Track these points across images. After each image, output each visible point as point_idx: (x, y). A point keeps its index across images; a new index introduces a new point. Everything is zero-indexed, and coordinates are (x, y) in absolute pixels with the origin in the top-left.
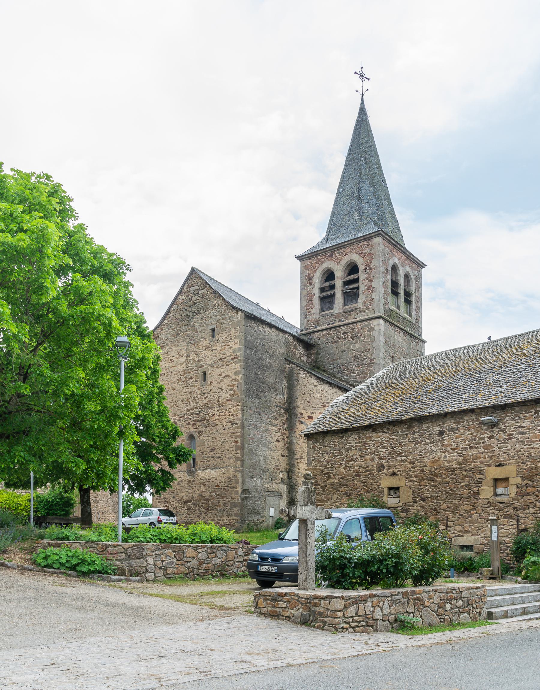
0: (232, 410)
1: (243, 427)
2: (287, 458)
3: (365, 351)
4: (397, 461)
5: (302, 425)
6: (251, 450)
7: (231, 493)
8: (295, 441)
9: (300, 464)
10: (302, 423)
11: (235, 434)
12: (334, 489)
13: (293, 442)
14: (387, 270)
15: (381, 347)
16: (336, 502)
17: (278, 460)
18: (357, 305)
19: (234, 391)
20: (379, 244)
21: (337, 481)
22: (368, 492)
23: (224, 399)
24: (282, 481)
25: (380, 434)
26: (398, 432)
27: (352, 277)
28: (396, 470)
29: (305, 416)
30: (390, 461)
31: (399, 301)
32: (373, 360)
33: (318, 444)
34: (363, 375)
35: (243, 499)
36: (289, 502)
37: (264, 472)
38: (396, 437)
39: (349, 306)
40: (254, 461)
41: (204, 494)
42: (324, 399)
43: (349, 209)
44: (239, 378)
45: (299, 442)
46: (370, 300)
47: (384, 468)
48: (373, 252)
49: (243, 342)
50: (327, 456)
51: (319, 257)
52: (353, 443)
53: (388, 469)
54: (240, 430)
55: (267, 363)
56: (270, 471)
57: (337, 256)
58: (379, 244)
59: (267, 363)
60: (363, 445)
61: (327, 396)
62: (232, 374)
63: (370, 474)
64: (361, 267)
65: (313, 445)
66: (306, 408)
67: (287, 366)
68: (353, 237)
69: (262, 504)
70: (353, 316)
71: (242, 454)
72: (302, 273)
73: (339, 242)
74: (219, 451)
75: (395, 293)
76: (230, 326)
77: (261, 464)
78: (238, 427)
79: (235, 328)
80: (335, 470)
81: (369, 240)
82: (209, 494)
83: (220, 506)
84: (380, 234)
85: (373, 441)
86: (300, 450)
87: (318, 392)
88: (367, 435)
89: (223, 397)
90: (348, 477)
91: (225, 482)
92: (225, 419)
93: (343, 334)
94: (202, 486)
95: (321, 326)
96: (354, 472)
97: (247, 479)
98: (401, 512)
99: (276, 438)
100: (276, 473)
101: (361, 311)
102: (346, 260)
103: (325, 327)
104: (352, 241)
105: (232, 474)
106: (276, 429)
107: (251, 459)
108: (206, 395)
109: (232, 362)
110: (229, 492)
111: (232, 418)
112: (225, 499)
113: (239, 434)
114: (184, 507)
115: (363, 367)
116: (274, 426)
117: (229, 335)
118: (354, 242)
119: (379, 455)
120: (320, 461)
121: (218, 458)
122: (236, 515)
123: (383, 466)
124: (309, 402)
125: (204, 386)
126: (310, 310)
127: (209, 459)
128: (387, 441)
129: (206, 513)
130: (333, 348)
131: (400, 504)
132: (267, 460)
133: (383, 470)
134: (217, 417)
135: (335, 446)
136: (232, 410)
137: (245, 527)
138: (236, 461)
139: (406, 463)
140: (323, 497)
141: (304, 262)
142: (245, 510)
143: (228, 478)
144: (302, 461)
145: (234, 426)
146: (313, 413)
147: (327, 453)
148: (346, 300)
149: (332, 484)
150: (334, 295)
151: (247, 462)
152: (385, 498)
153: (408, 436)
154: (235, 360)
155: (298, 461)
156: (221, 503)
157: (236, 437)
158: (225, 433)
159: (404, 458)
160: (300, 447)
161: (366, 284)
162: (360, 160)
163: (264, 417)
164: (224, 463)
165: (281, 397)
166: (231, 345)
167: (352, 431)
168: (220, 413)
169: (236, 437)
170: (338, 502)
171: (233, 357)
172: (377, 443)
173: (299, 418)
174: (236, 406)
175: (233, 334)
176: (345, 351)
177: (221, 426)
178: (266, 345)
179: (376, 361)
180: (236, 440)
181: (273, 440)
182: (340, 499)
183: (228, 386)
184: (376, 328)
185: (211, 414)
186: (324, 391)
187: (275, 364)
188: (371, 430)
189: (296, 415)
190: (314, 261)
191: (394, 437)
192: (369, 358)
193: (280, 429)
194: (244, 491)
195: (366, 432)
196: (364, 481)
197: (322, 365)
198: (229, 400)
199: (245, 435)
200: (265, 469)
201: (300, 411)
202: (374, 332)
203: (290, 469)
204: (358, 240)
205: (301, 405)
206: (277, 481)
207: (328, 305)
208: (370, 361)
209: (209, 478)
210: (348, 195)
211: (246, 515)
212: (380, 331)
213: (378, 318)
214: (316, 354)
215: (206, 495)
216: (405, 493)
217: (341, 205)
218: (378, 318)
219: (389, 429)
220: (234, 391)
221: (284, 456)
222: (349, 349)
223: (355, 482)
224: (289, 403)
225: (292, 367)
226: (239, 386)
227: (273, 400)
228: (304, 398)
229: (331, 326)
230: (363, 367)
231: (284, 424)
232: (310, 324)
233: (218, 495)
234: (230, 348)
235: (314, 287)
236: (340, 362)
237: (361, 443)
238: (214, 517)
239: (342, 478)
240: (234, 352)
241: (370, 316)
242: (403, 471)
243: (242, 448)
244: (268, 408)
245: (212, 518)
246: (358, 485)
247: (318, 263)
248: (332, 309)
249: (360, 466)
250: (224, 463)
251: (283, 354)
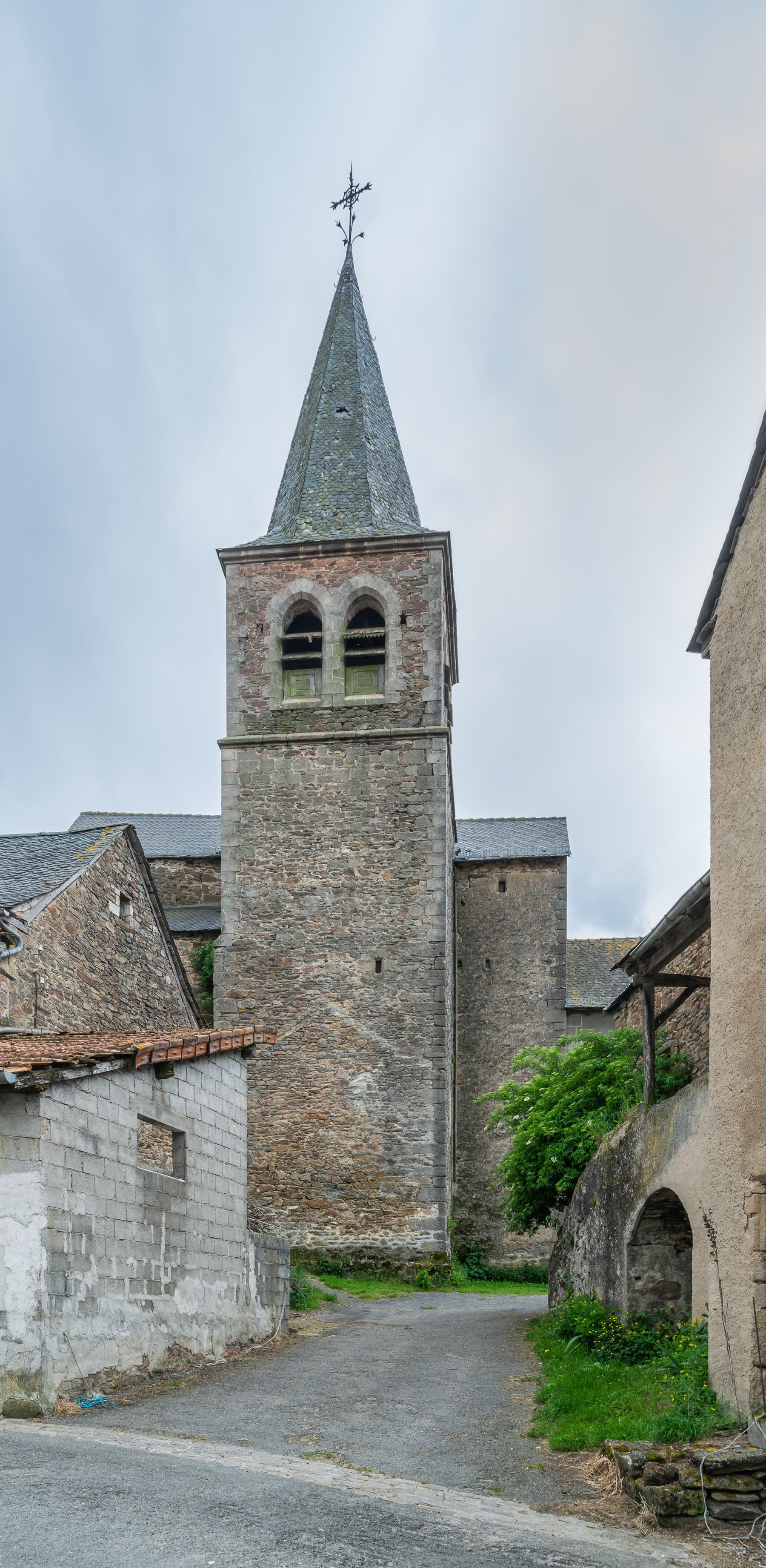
64: (392, 619)
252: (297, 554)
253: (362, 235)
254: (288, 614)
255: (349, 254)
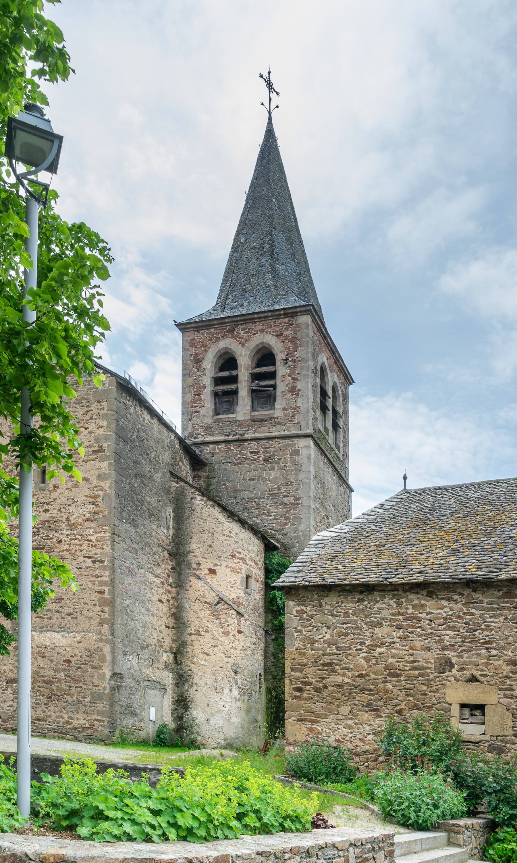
0: (93, 538)
1: (113, 569)
2: (174, 631)
3: (285, 484)
4: (479, 655)
5: (199, 581)
6: (125, 609)
7: (92, 677)
8: (188, 606)
9: (196, 643)
10: (199, 578)
11: (98, 579)
12: (343, 694)
13: (183, 607)
14: (316, 368)
15: (311, 481)
16: (347, 719)
17: (161, 632)
18: (272, 412)
19: (97, 506)
20: (308, 325)
21: (350, 681)
22: (416, 707)
23: (78, 517)
24: (166, 667)
25: (444, 603)
26: (482, 602)
27: (264, 369)
28: (477, 674)
29: (205, 567)
30: (465, 656)
31: (327, 422)
32: (299, 499)
33: (309, 608)
34: (283, 520)
35: (113, 689)
36: (177, 701)
37: (142, 648)
38: (478, 612)
39: (260, 413)
40: (129, 627)
41: (42, 672)
42: (234, 546)
43: (257, 268)
44: (106, 485)
45: (194, 608)
46: (293, 408)
47: (452, 666)
48: (298, 336)
49: (114, 426)
50: (329, 631)
51: (212, 330)
52: (385, 613)
53: (462, 669)
54: (107, 573)
55: (147, 472)
56: (150, 648)
57: (242, 333)
58: (308, 325)
59: (147, 472)
60: (407, 619)
61: (237, 542)
62: (93, 478)
63: (420, 675)
64: (280, 357)
65: (297, 608)
66: (206, 556)
67: (174, 484)
68: (267, 309)
69: (140, 699)
70: (266, 429)
71: (112, 614)
72: (184, 350)
73: (244, 312)
74: (70, 604)
75: (324, 408)
76: (91, 396)
77: (138, 635)
78: (104, 568)
79: (99, 401)
80: (346, 660)
81: (293, 317)
82: (52, 673)
83: (72, 695)
84: (310, 310)
85: (428, 614)
86: (196, 621)
87: (225, 532)
88: (416, 602)
89: (77, 515)
90: (373, 676)
91: (81, 656)
92: (81, 551)
93: (251, 453)
94: (39, 659)
95: (215, 435)
96: (387, 667)
97: (120, 657)
98: (488, 752)
99: (158, 597)
100: (159, 652)
101: (279, 423)
102: (255, 341)
103: (223, 438)
104: (266, 314)
105: (93, 646)
106: (158, 581)
107: (125, 625)
108: (46, 507)
109: (93, 457)
110: (88, 673)
111: (94, 551)
112: (80, 684)
113: (106, 579)
114: (6, 689)
115: (283, 509)
116: (156, 576)
117: (88, 411)
118: (269, 317)
119: (441, 641)
120: (314, 641)
121: (69, 614)
122: (100, 713)
123: (451, 662)
124: (210, 546)
125: (42, 490)
126: (198, 409)
127: (51, 615)
128: (459, 617)
129: (46, 704)
130: (234, 471)
131: (487, 738)
132: (146, 629)
133: (450, 671)
134: (67, 547)
135: (346, 614)
136: (93, 538)
137: (117, 734)
138: (100, 624)
139: (500, 662)
140: (318, 707)
141: (188, 334)
142: (117, 708)
143: (86, 650)
144: (199, 638)
145: (97, 565)
146: (216, 565)
147: (329, 627)
148: (255, 405)
149: (338, 686)
150: (235, 392)
151: (118, 627)
152: (454, 722)
153: (504, 612)
154: (99, 455)
155: (193, 637)
156: (73, 690)
157: (101, 583)
158: (81, 575)
159: (494, 652)
160: (196, 615)
161: (287, 382)
162: (272, 201)
163: (143, 558)
164: (78, 624)
165: (165, 531)
166: (91, 429)
167: (384, 591)
168: (71, 539)
169: (101, 583)
170: (351, 719)
171: (96, 448)
172: (437, 619)
173: (194, 569)
174: (100, 532)
175: (95, 411)
176: (254, 480)
177: (74, 562)
178: (145, 441)
179: (304, 502)
180: (100, 588)
181: (155, 599)
182: (356, 715)
183: (87, 496)
184: (304, 452)
185: (55, 540)
186: (234, 533)
187: (158, 476)
188: (425, 593)
189: (189, 565)
190: (204, 335)
191: (473, 611)
192: (293, 496)
193: (163, 583)
194: (115, 675)
195: (412, 596)
196: (407, 686)
197: (217, 496)
198: (88, 520)
199: (117, 582)
200: (144, 645)
201: (196, 559)
202: (300, 457)
203: (178, 649)
204: (276, 314)
205: (197, 550)
206: (160, 667)
207: (225, 406)
208: (295, 500)
209: (53, 646)
210: (254, 248)
211: (118, 716)
212: (309, 457)
213: (306, 436)
214: (208, 477)
215: (47, 674)
216: (498, 717)
217: (245, 259)
218: (306, 436)
219: (463, 595)
220: (97, 506)
221: (168, 627)
222: (259, 478)
223: (389, 686)
224: (178, 544)
225: (181, 487)
226: (106, 498)
227: (154, 534)
228: (203, 540)
229: (231, 438)
230: (283, 509)
231: (169, 576)
232: (197, 430)
233: (69, 677)
234: (90, 433)
235: (205, 374)
236: (246, 494)
237: (403, 615)
238: (62, 712)
239: (360, 676)
240: (97, 440)
241: (294, 432)
242: (492, 676)
243: (111, 603)
244: (148, 545)
245: (58, 714)
246: (396, 691)
247: (210, 340)
248: (233, 413)
249: (400, 658)
250: (78, 624)
251: (167, 464)
252: (214, 325)
253: (277, 107)
254: (216, 364)
255: (270, 119)
